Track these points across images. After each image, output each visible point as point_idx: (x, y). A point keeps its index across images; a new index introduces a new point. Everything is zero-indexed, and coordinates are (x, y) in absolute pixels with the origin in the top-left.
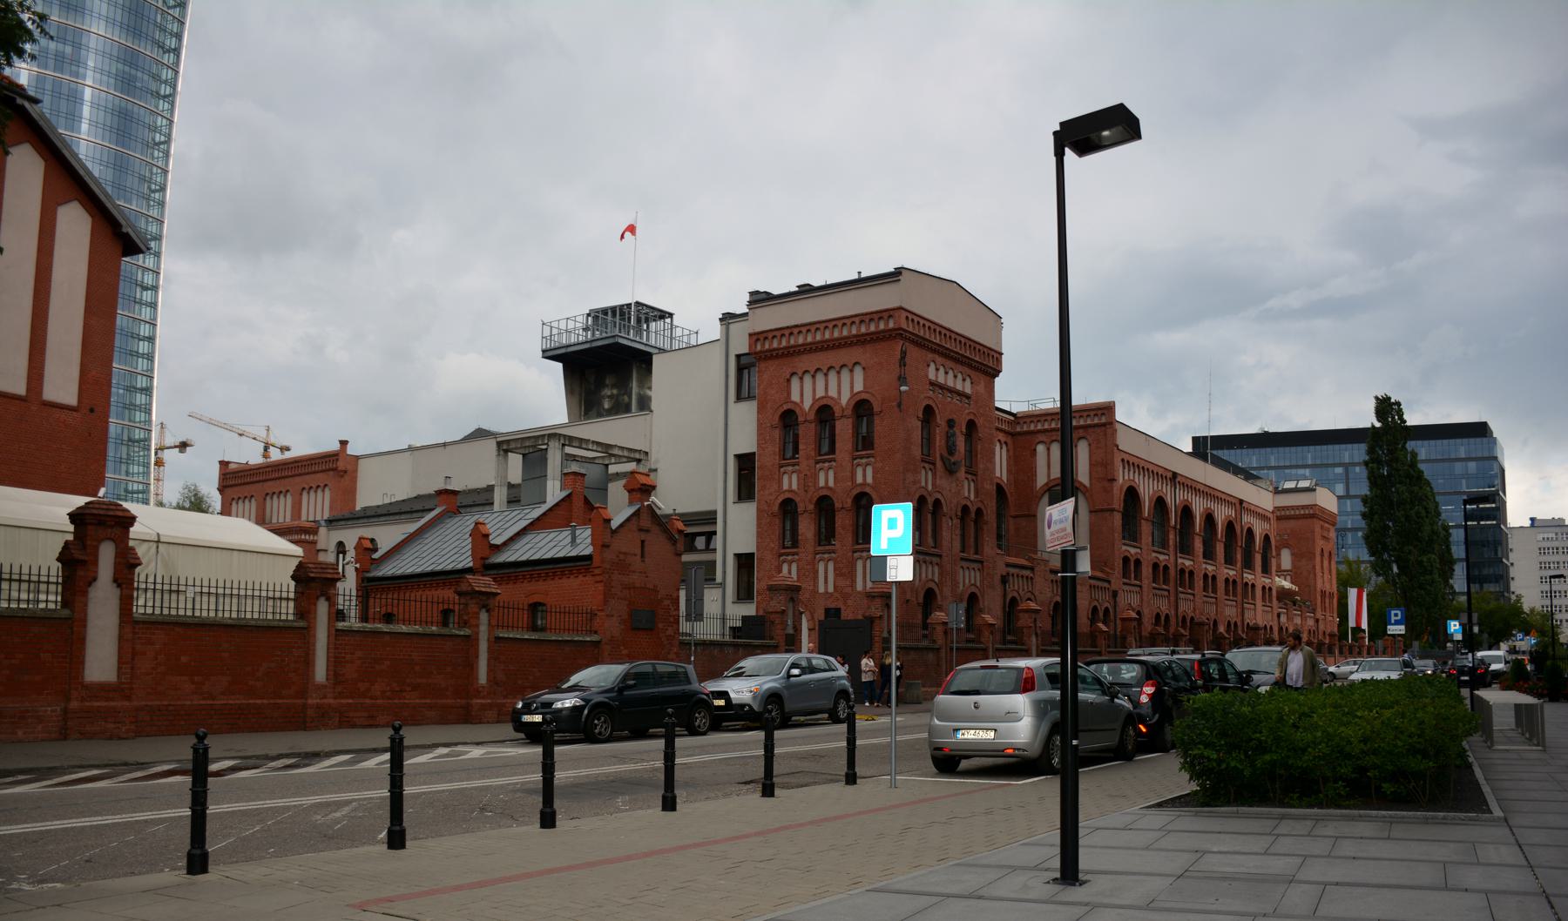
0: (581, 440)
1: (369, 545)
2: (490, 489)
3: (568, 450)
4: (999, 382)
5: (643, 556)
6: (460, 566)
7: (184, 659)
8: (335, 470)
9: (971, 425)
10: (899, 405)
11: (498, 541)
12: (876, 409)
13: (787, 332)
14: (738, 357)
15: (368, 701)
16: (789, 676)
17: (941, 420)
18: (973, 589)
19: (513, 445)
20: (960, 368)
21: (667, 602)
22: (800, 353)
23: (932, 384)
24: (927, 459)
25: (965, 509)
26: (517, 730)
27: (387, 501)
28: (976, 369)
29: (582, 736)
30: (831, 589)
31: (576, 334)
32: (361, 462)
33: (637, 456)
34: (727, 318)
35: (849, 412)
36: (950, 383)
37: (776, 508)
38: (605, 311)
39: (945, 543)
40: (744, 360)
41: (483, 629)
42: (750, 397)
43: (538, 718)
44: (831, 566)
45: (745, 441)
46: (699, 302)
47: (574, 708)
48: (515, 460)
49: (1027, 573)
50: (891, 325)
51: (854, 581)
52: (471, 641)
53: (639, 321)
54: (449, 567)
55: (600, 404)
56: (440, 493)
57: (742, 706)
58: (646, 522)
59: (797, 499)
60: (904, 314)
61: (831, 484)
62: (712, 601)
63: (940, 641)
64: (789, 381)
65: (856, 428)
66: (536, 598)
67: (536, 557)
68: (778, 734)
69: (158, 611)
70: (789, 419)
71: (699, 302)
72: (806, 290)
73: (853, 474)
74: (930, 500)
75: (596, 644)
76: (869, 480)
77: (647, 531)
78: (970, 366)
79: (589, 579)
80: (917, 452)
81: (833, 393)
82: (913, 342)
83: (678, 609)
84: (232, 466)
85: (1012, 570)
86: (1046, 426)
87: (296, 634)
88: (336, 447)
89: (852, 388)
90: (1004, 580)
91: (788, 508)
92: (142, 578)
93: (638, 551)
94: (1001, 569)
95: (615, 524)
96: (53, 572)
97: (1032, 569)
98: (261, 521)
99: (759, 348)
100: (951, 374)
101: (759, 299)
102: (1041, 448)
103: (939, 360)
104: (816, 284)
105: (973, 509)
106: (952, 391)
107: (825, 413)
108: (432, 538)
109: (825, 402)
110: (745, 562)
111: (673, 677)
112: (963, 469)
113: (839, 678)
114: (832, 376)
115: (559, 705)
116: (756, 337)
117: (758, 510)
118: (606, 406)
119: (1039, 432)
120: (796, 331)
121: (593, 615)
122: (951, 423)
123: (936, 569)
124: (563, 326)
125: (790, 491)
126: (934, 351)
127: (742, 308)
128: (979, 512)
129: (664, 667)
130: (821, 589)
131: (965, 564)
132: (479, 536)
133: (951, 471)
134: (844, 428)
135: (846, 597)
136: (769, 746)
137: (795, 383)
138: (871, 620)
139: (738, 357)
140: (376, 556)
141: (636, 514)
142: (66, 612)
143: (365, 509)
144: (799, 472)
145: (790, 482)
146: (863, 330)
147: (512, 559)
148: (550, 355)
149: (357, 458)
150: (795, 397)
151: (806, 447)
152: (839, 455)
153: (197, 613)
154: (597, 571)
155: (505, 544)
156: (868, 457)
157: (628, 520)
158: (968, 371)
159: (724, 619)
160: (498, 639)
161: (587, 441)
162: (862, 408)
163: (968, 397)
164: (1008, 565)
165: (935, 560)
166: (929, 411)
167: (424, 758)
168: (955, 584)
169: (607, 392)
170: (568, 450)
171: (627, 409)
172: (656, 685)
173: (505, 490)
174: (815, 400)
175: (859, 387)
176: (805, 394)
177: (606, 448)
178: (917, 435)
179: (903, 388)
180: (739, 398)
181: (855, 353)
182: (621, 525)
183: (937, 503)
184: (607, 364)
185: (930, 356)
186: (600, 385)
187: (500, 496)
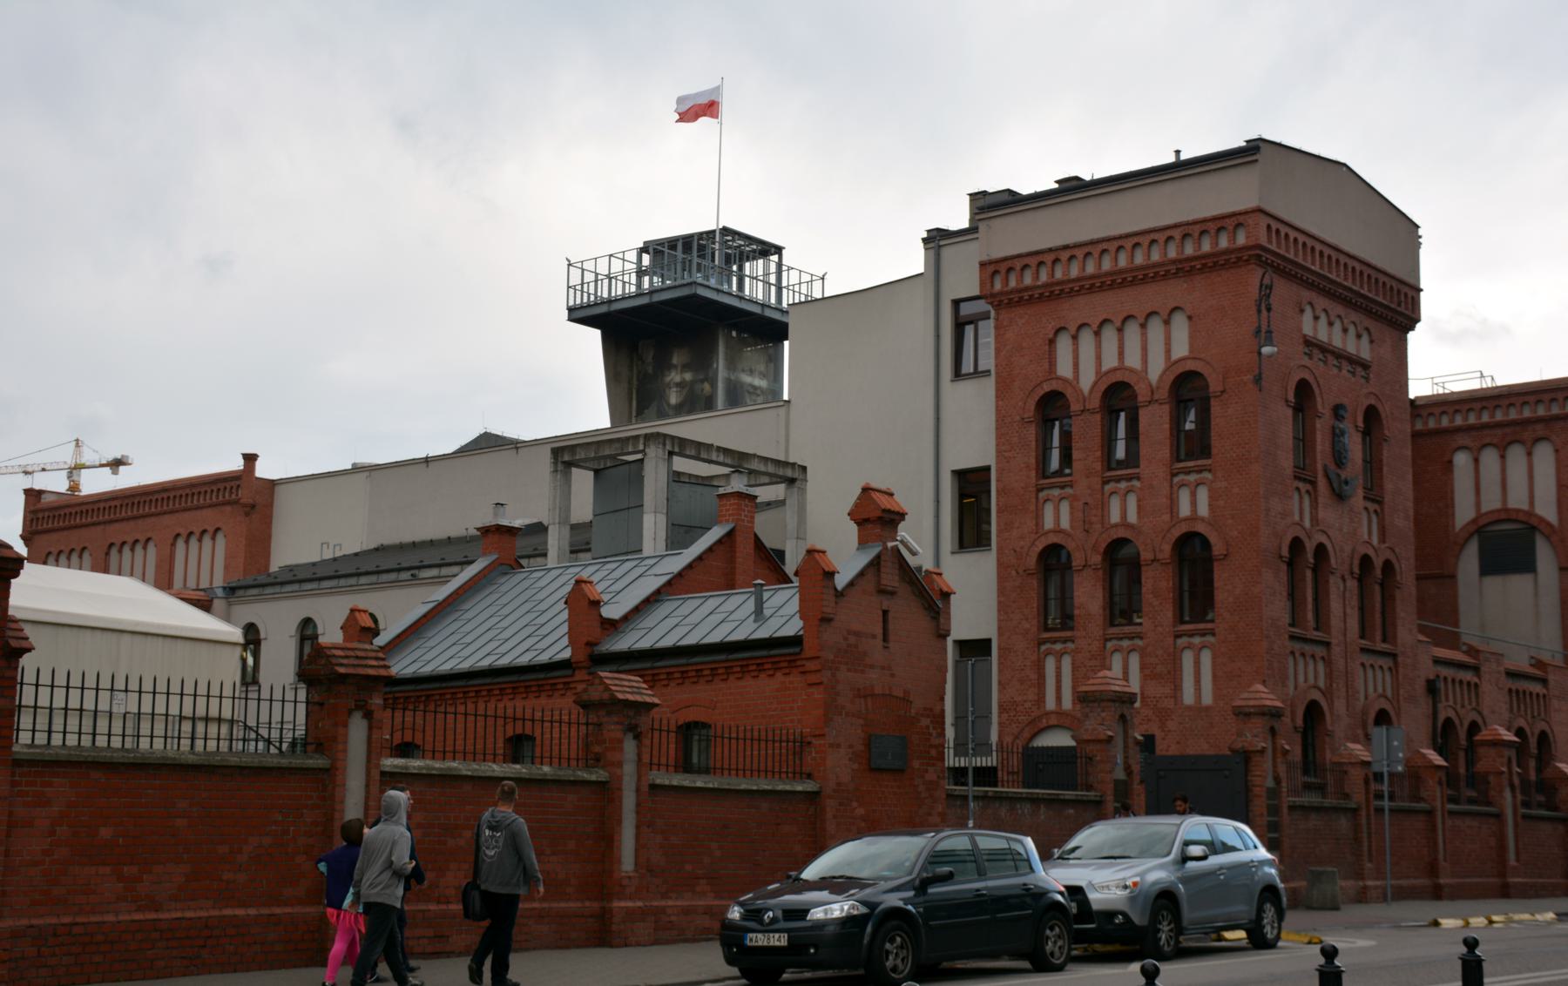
0: (699, 445)
1: (369, 623)
2: (539, 529)
3: (681, 464)
5: (885, 639)
6: (544, 658)
7: (105, 833)
8: (236, 502)
9: (1372, 414)
10: (1258, 379)
12: (1214, 386)
13: (1049, 258)
14: (956, 303)
15: (433, 907)
16: (1185, 859)
17: (1323, 405)
19: (581, 455)
20: (1354, 316)
21: (925, 722)
22: (1072, 293)
23: (1308, 342)
24: (1303, 474)
25: (1366, 561)
26: (730, 961)
27: (328, 555)
28: (1378, 317)
29: (1026, 964)
30: (1207, 699)
31: (625, 282)
32: (279, 490)
33: (789, 473)
34: (936, 239)
35: (1163, 394)
36: (1337, 342)
37: (1032, 561)
38: (672, 243)
39: (1336, 622)
40: (966, 309)
41: (629, 769)
42: (977, 373)
43: (779, 940)
45: (973, 443)
46: (849, 228)
47: (848, 921)
48: (583, 480)
49: (1468, 676)
50: (1241, 240)
52: (606, 792)
53: (728, 260)
54: (524, 660)
55: (663, 397)
56: (485, 531)
57: (1109, 915)
58: (890, 578)
59: (1071, 545)
60: (1264, 221)
61: (1132, 517)
63: (1358, 797)
64: (1052, 342)
65: (1177, 421)
66: (692, 715)
67: (691, 640)
69: (41, 739)
70: (1052, 406)
71: (849, 228)
72: (1072, 188)
73: (1039, 517)
74: (1310, 546)
75: (812, 797)
76: (1203, 510)
77: (893, 593)
78: (1369, 313)
79: (796, 679)
80: (1287, 462)
81: (1133, 360)
82: (1278, 270)
83: (942, 734)
84: (46, 499)
85: (1446, 672)
86: (1472, 420)
87: (307, 772)
88: (237, 464)
89: (1168, 351)
90: (1432, 688)
91: (1053, 561)
92: (29, 677)
93: (879, 630)
94: (1427, 670)
95: (841, 581)
97: (1476, 669)
98: (164, 582)
99: (998, 286)
100: (1338, 326)
101: (988, 206)
102: (1461, 460)
103: (1321, 302)
104: (1025, 190)
105: (1378, 563)
106: (1341, 356)
107: (1118, 396)
108: (478, 611)
109: (1119, 377)
111: (997, 856)
112: (1360, 493)
113: (1263, 863)
114: (1132, 331)
115: (817, 914)
116: (991, 268)
117: (1002, 567)
118: (674, 399)
119: (1458, 430)
120: (1065, 255)
121: (803, 744)
122: (1338, 411)
124: (603, 270)
125: (1058, 531)
126: (1311, 286)
127: (959, 219)
128: (1388, 566)
129: (990, 841)
131: (1368, 659)
132: (582, 603)
133: (1340, 496)
134: (1156, 421)
137: (1064, 346)
138: (1246, 757)
139: (956, 303)
140: (380, 641)
141: (875, 563)
142: (1545, 556)
143: (291, 568)
144: (1073, 499)
145: (1058, 516)
146: (1189, 250)
148: (580, 315)
149: (272, 484)
150: (1064, 368)
151: (1086, 455)
152: (1145, 469)
153: (101, 741)
154: (810, 666)
155: (626, 618)
156: (1129, 478)
157: (861, 574)
158: (1368, 323)
160: (654, 787)
161: (709, 447)
162: (1187, 388)
163: (1365, 366)
164: (1438, 661)
165: (1320, 651)
166: (1304, 389)
169: (675, 377)
170: (681, 464)
171: (709, 404)
172: (981, 874)
173: (566, 531)
174: (1100, 375)
175: (1181, 349)
176: (1082, 364)
177: (739, 460)
178: (1286, 432)
179: (1266, 350)
180: (958, 374)
181: (1174, 292)
182: (851, 584)
183: (1321, 550)
184: (681, 324)
185: (1306, 294)
186: (663, 365)
187: (555, 541)
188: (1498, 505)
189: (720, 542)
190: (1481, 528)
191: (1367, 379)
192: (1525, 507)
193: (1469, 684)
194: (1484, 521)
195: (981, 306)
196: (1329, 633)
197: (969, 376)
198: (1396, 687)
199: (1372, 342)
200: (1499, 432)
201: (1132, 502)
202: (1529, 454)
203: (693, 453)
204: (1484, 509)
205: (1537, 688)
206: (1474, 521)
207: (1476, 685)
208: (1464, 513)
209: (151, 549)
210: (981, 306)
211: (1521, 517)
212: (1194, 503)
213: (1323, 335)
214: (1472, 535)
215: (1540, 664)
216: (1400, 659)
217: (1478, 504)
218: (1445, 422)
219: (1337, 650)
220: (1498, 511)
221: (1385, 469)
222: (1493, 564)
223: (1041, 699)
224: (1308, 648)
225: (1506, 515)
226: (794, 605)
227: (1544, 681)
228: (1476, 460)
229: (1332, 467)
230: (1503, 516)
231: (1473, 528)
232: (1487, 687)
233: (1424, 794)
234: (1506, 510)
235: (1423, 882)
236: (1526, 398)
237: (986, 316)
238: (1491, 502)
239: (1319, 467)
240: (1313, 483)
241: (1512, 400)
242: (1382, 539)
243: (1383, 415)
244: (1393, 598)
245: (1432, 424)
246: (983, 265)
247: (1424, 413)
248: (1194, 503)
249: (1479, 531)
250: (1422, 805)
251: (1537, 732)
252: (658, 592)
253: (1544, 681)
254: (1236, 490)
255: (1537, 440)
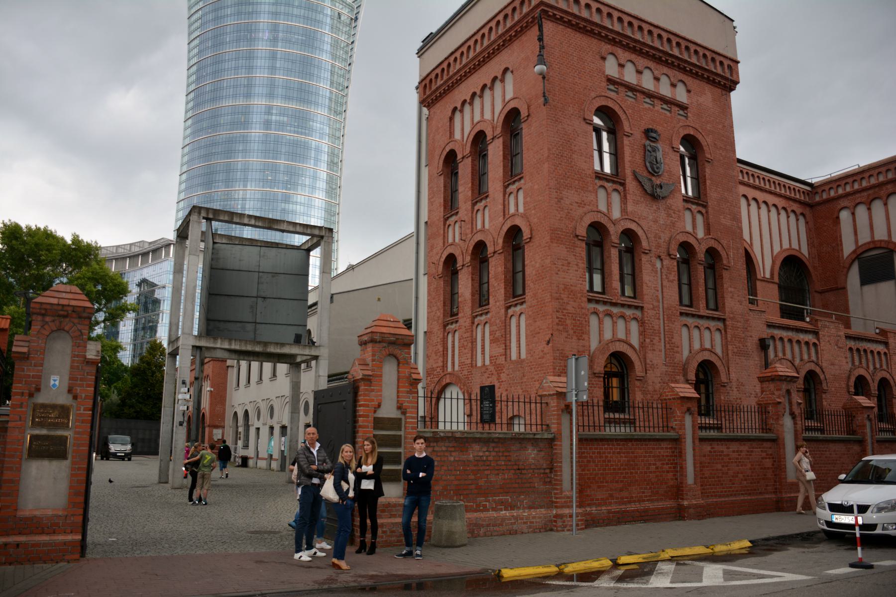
4: (735, 96)
10: (546, 102)
18: (706, 356)
23: (610, 81)
49: (810, 338)
51: (507, 347)
64: (451, 119)
74: (615, 233)
78: (684, 70)
85: (777, 333)
90: (763, 345)
97: (816, 333)
102: (845, 215)
104: (434, 31)
119: (840, 197)
123: (634, 327)
126: (613, 42)
135: (499, 368)
163: (683, 107)
167: (70, 537)
168: (672, 348)
183: (712, 253)
185: (606, 47)
188: (868, 239)
190: (858, 256)
191: (686, 117)
192: (886, 238)
193: (879, 353)
194: (861, 250)
196: (642, 299)
198: (725, 347)
199: (689, 91)
200: (865, 194)
202: (886, 204)
203: (226, 218)
204: (860, 244)
205: (881, 348)
206: (854, 252)
207: (815, 344)
208: (848, 247)
211: (883, 245)
213: (630, 76)
214: (853, 261)
215: (883, 332)
216: (727, 323)
217: (856, 241)
218: (832, 193)
219: (650, 313)
220: (869, 243)
221: (708, 182)
222: (867, 279)
223: (445, 366)
224: (615, 310)
225: (874, 245)
227: (886, 344)
228: (853, 214)
229: (643, 174)
230: (872, 246)
231: (854, 256)
232: (823, 345)
233: (674, 424)
234: (873, 242)
235: (669, 503)
236: (880, 170)
238: (864, 238)
239: (628, 172)
240: (623, 184)
241: (871, 173)
242: (708, 229)
243: (704, 143)
244: (721, 277)
245: (825, 196)
247: (819, 191)
249: (858, 257)
250: (672, 434)
251: (878, 378)
253: (886, 344)
254: (536, 187)
255: (889, 195)
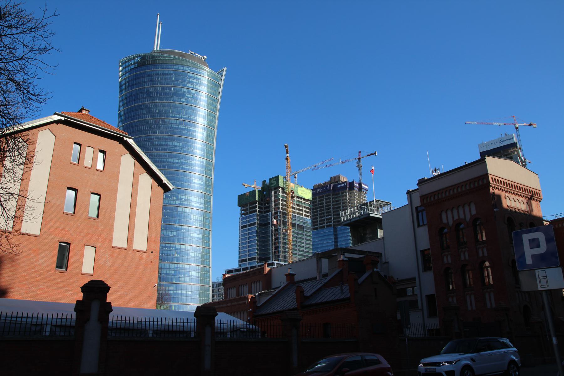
11: (308, 294)
30: (474, 308)
34: (409, 193)
40: (419, 209)
42: (424, 225)
44: (473, 297)
45: (425, 243)
62: (415, 318)
64: (441, 215)
68: (333, 248)
81: (462, 216)
96: (193, 321)
110: (430, 298)
116: (423, 198)
130: (470, 308)
136: (336, 242)
139: (417, 208)
145: (448, 259)
147: (314, 302)
150: (445, 221)
155: (311, 295)
159: (424, 326)
175: (474, 212)
176: (448, 218)
189: (338, 273)
195: (422, 208)
197: (422, 226)
201: (467, 254)
209: (247, 286)
210: (422, 208)
212: (483, 253)
226: (348, 287)
237: (423, 210)
246: (420, 197)
248: (483, 253)
252: (321, 288)
